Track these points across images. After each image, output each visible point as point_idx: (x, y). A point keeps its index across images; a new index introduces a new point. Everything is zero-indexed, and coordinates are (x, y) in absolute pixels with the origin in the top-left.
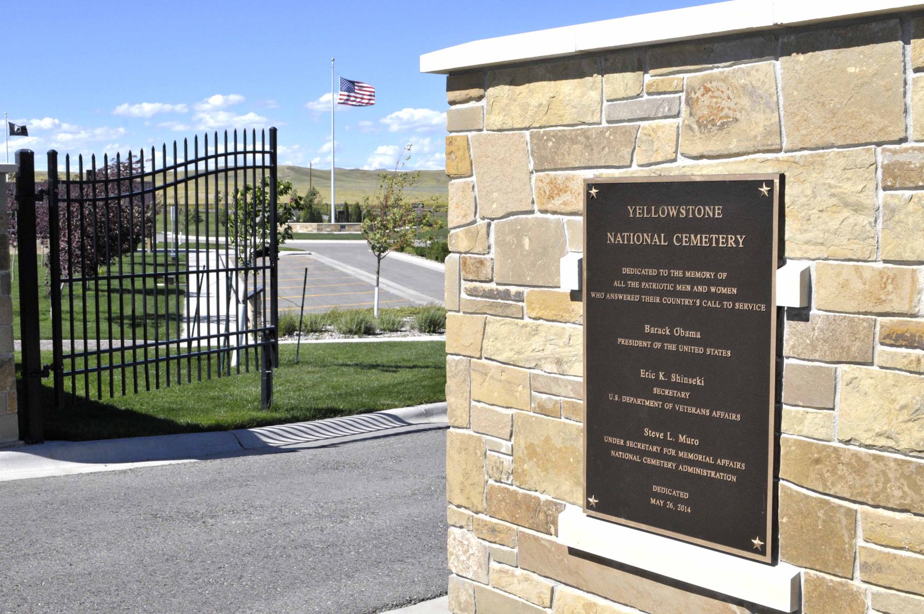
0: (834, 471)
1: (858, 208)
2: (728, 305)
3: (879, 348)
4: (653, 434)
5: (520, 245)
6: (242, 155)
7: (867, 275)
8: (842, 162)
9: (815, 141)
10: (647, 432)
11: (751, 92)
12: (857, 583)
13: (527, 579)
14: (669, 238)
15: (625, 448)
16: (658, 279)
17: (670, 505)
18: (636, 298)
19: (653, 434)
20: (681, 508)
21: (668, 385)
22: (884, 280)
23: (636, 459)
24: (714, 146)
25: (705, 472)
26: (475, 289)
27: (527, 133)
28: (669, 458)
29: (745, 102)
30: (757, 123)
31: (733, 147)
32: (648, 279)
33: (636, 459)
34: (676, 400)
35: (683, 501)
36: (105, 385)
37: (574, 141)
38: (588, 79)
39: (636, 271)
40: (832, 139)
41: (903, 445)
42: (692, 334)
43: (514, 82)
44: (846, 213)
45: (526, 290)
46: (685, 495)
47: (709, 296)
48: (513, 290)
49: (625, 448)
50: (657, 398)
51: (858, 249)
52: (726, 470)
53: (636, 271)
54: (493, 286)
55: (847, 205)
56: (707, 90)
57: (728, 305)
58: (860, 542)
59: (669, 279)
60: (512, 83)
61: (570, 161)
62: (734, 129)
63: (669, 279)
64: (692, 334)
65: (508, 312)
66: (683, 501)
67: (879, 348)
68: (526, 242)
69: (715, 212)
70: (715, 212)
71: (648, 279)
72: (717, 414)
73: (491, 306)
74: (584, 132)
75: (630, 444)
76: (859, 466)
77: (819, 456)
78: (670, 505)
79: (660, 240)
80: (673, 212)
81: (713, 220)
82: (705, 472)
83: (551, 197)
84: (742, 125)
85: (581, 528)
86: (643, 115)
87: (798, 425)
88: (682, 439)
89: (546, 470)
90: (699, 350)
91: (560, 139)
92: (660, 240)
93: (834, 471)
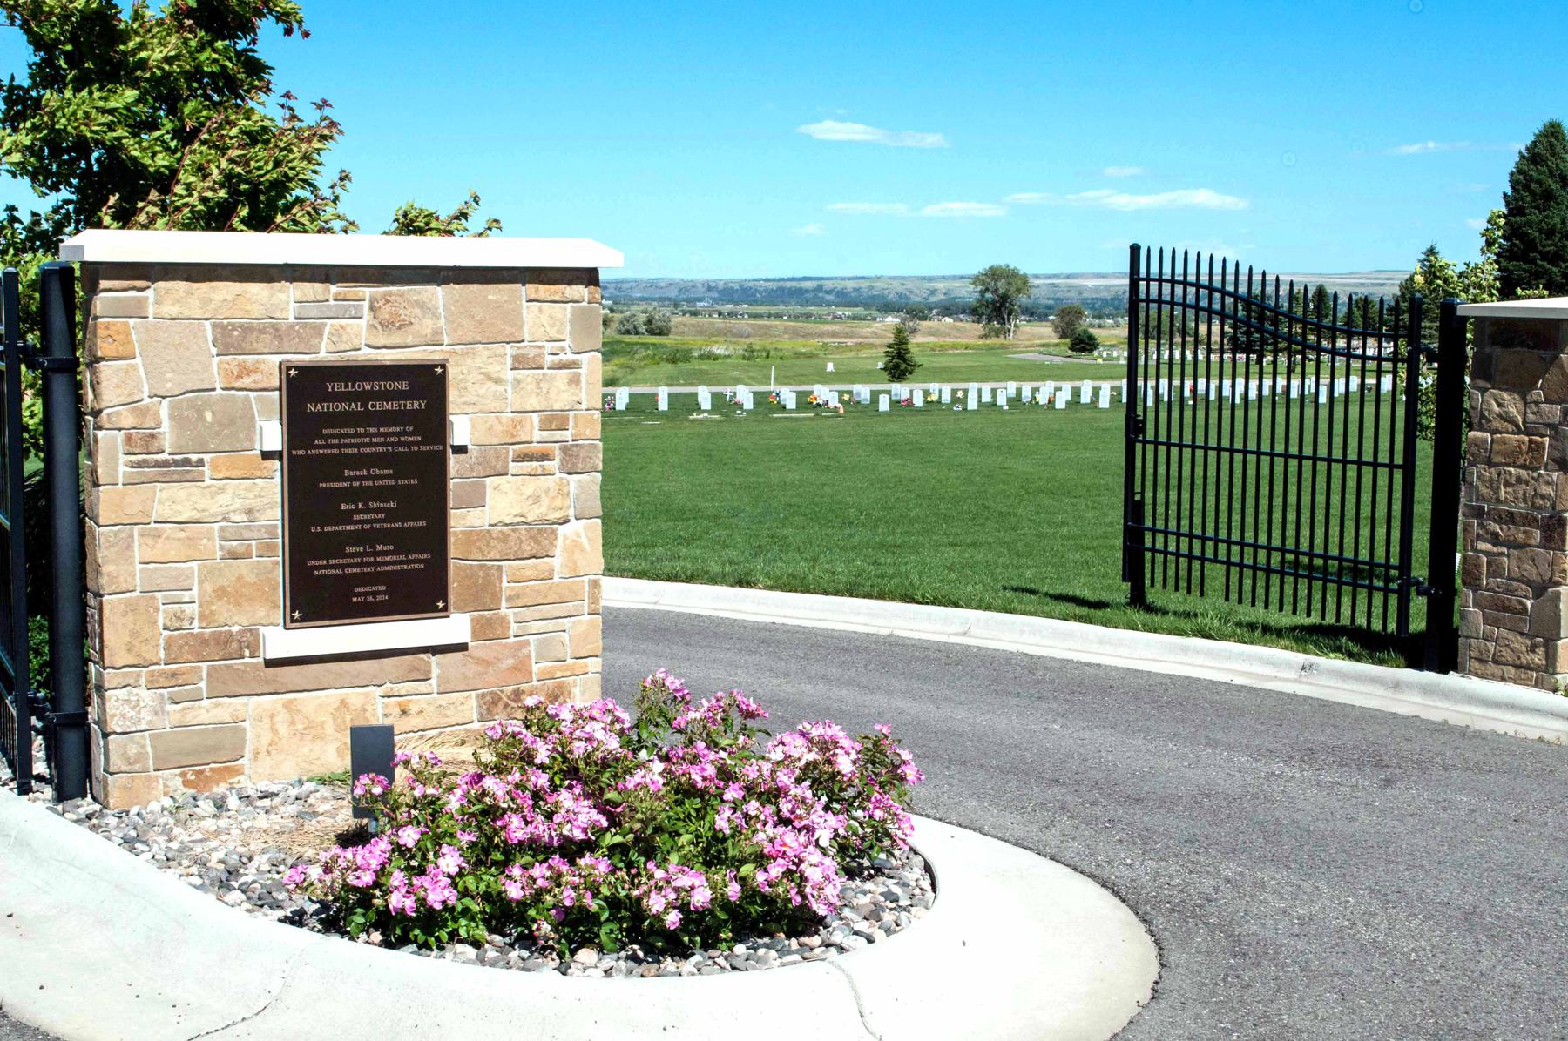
0: (488, 545)
1: (497, 381)
2: (415, 448)
3: (511, 465)
4: (353, 550)
5: (201, 418)
6: (1365, 459)
7: (504, 421)
8: (486, 353)
9: (469, 339)
10: (348, 550)
11: (421, 305)
12: (503, 611)
13: (217, 705)
14: (364, 405)
15: (323, 568)
16: (357, 435)
17: (370, 598)
18: (336, 451)
19: (353, 550)
20: (379, 598)
21: (367, 511)
22: (515, 424)
23: (339, 571)
24: (396, 339)
25: (398, 567)
26: (144, 461)
27: (207, 324)
28: (369, 564)
29: (417, 311)
30: (426, 326)
31: (410, 341)
32: (347, 436)
33: (339, 571)
34: (376, 521)
35: (381, 593)
36: (1422, 521)
37: (262, 331)
38: (277, 285)
39: (336, 431)
40: (479, 338)
41: (530, 519)
42: (386, 472)
43: (189, 279)
44: (490, 384)
45: (206, 457)
46: (383, 588)
47: (399, 444)
48: (194, 457)
49: (323, 568)
50: (356, 522)
51: (497, 406)
52: (416, 561)
53: (336, 431)
54: (165, 456)
55: (490, 379)
56: (387, 301)
57: (415, 448)
58: (505, 584)
59: (366, 435)
60: (187, 280)
61: (259, 347)
62: (409, 329)
63: (366, 435)
64: (386, 472)
65: (189, 477)
66: (381, 593)
67: (511, 465)
68: (208, 416)
69: (404, 386)
70: (404, 386)
71: (347, 436)
72: (326, 529)
73: (165, 474)
74: (272, 326)
75: (332, 562)
76: (504, 538)
77: (475, 536)
78: (370, 598)
79: (356, 407)
80: (368, 386)
81: (401, 392)
82: (398, 567)
83: (239, 377)
84: (416, 327)
85: (283, 641)
86: (329, 314)
87: (460, 520)
88: (379, 548)
89: (239, 605)
90: (393, 482)
91: (246, 330)
92: (356, 407)
93: (488, 545)
